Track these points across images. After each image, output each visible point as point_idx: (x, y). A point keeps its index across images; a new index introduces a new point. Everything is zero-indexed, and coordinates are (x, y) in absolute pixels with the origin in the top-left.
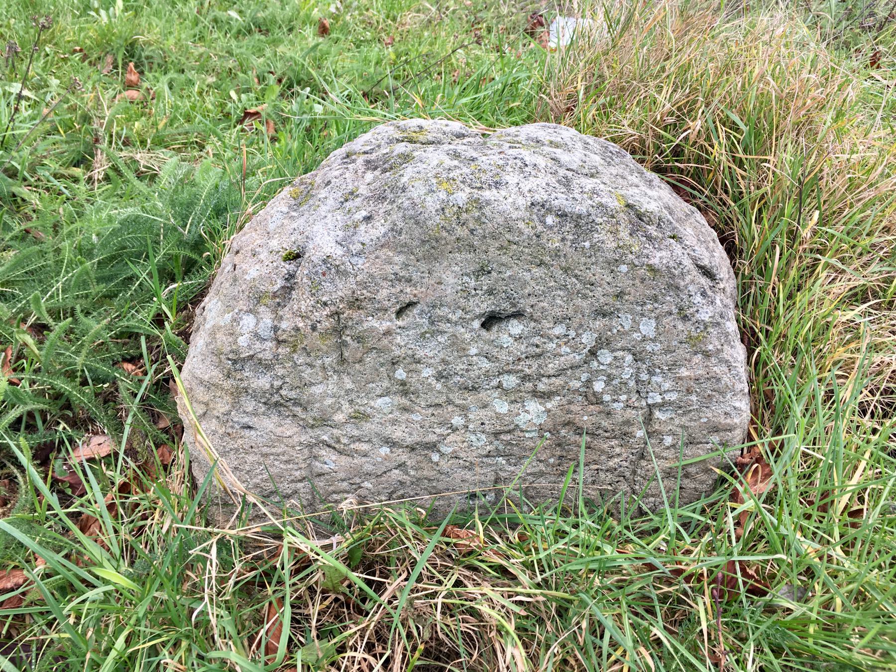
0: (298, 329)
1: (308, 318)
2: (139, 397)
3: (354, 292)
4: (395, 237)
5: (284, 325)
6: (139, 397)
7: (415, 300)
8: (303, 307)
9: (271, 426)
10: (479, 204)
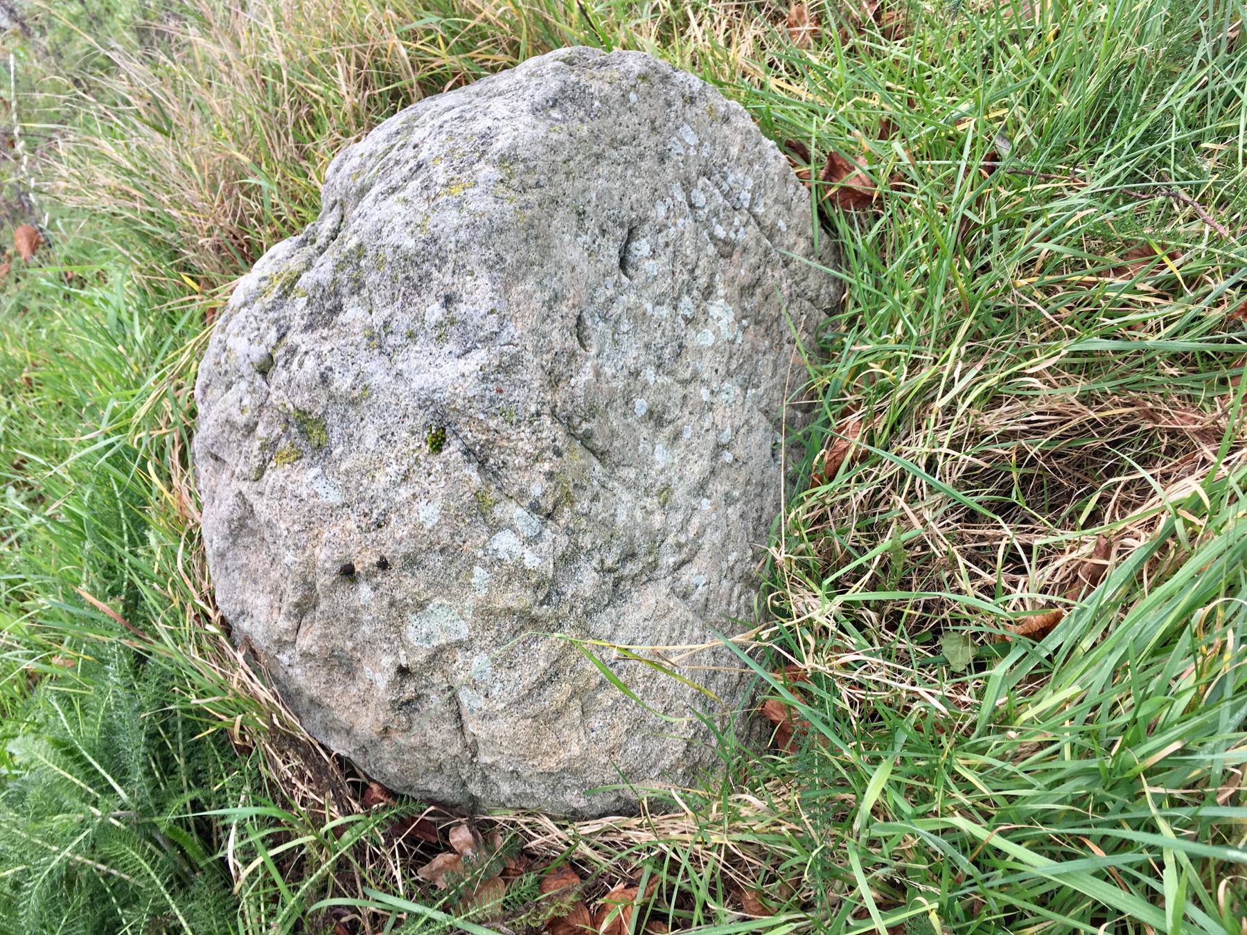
0: (550, 475)
1: (543, 451)
2: (1134, 464)
3: (542, 367)
4: (502, 270)
5: (536, 490)
6: (1134, 464)
7: (577, 312)
8: (527, 447)
9: (637, 616)
10: (506, 160)
